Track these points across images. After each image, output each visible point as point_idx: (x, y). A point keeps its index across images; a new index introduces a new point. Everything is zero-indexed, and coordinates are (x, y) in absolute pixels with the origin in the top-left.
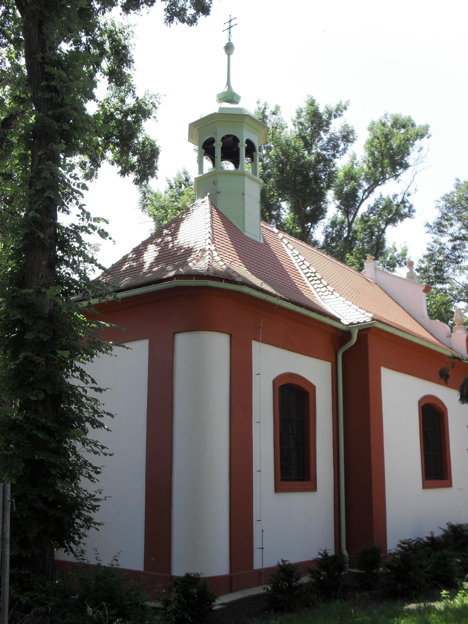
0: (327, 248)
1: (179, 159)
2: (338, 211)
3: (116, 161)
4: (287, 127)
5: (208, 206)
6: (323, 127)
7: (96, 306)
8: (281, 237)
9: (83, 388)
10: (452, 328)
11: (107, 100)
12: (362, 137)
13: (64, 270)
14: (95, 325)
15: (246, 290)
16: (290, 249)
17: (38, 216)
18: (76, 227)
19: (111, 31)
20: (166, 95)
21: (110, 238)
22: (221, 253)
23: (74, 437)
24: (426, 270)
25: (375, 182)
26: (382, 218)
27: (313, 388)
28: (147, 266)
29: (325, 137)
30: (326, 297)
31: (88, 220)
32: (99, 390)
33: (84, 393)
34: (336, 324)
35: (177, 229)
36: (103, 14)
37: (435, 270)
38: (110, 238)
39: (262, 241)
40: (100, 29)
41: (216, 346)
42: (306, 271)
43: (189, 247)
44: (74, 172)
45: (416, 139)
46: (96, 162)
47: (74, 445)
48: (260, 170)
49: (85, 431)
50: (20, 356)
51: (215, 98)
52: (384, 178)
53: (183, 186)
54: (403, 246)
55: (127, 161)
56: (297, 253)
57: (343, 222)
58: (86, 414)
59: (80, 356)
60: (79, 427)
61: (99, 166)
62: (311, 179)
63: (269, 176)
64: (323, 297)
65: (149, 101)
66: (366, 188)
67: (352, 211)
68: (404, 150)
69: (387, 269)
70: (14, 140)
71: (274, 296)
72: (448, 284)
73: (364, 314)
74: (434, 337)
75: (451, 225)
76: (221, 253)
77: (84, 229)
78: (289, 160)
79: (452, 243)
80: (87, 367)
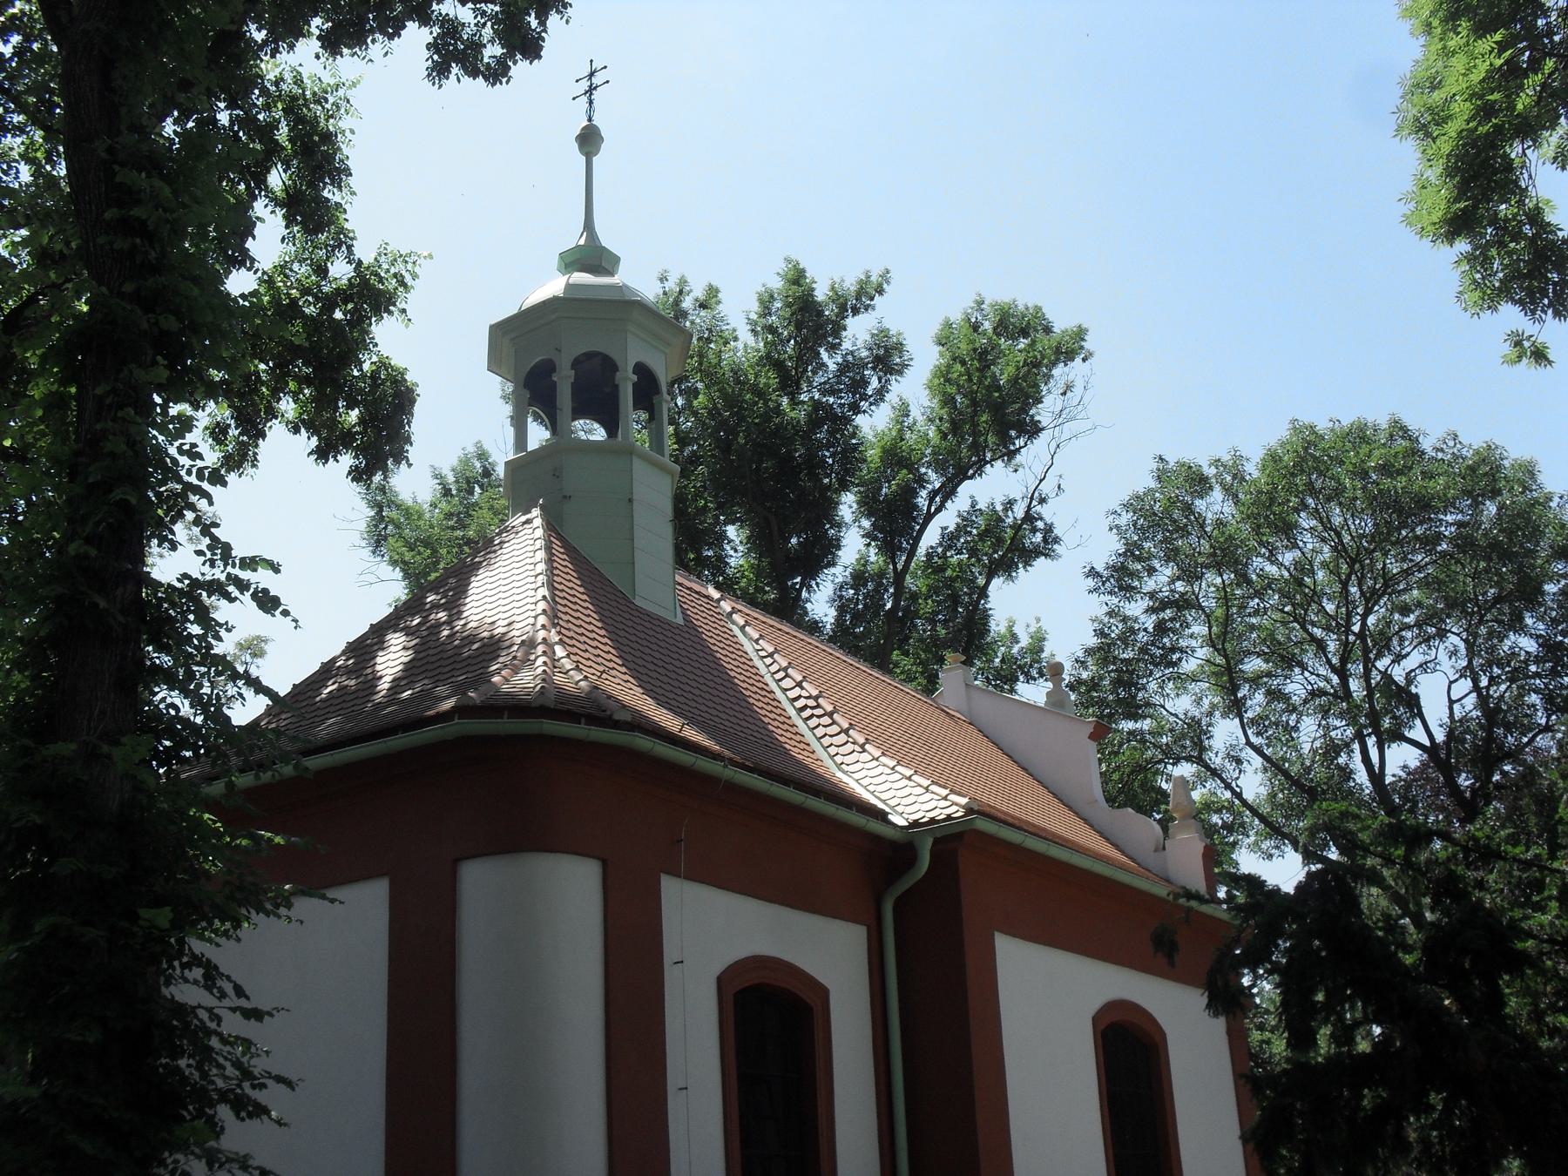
0: (844, 637)
1: (463, 416)
2: (868, 545)
3: (303, 421)
4: (736, 339)
5: (539, 533)
6: (825, 336)
7: (248, 792)
8: (729, 609)
9: (210, 1010)
10: (1165, 830)
11: (283, 268)
12: (924, 359)
13: (167, 697)
14: (244, 842)
15: (643, 742)
16: (751, 639)
17: (93, 552)
18: (195, 584)
19: (294, 98)
20: (430, 256)
21: (286, 613)
22: (575, 650)
23: (184, 1147)
24: (1093, 684)
25: (958, 471)
26: (979, 560)
27: (823, 993)
28: (384, 685)
29: (831, 362)
30: (847, 759)
31: (225, 566)
32: (255, 1014)
33: (213, 1025)
34: (875, 826)
35: (462, 590)
36: (273, 56)
37: (1118, 683)
38: (286, 613)
39: (680, 620)
40: (264, 92)
41: (571, 889)
42: (792, 694)
43: (492, 637)
44: (190, 438)
45: (1054, 364)
46: (255, 426)
47: (187, 1168)
48: (670, 444)
49: (216, 1130)
50: (37, 929)
51: (555, 261)
52: (980, 461)
53: (477, 489)
54: (1032, 629)
55: (333, 423)
56: (771, 649)
57: (881, 574)
58: (220, 1083)
59: (204, 924)
60: (198, 1117)
61: (262, 435)
62: (799, 465)
63: (694, 460)
64: (839, 759)
65: (388, 271)
66: (937, 485)
67: (904, 545)
68: (1027, 390)
69: (996, 686)
70: (32, 359)
71: (715, 756)
72: (1148, 721)
73: (945, 798)
74: (1123, 853)
75: (1151, 571)
76: (575, 650)
77: (216, 588)
78: (742, 419)
79: (1154, 617)
80: (224, 954)
